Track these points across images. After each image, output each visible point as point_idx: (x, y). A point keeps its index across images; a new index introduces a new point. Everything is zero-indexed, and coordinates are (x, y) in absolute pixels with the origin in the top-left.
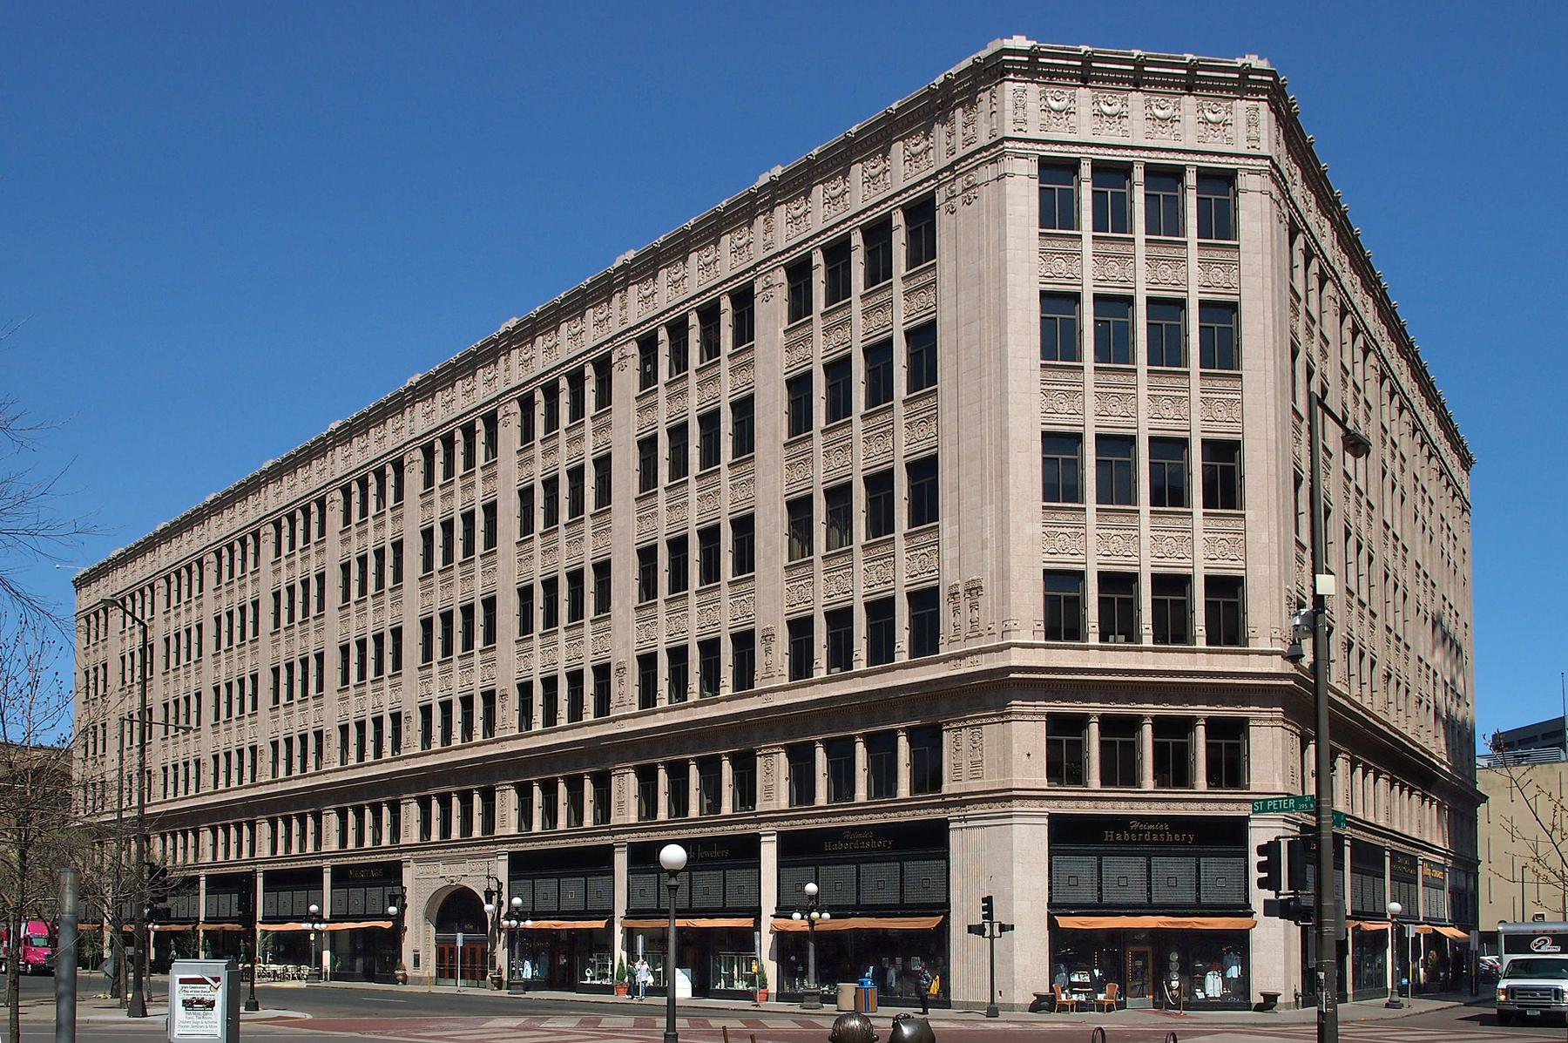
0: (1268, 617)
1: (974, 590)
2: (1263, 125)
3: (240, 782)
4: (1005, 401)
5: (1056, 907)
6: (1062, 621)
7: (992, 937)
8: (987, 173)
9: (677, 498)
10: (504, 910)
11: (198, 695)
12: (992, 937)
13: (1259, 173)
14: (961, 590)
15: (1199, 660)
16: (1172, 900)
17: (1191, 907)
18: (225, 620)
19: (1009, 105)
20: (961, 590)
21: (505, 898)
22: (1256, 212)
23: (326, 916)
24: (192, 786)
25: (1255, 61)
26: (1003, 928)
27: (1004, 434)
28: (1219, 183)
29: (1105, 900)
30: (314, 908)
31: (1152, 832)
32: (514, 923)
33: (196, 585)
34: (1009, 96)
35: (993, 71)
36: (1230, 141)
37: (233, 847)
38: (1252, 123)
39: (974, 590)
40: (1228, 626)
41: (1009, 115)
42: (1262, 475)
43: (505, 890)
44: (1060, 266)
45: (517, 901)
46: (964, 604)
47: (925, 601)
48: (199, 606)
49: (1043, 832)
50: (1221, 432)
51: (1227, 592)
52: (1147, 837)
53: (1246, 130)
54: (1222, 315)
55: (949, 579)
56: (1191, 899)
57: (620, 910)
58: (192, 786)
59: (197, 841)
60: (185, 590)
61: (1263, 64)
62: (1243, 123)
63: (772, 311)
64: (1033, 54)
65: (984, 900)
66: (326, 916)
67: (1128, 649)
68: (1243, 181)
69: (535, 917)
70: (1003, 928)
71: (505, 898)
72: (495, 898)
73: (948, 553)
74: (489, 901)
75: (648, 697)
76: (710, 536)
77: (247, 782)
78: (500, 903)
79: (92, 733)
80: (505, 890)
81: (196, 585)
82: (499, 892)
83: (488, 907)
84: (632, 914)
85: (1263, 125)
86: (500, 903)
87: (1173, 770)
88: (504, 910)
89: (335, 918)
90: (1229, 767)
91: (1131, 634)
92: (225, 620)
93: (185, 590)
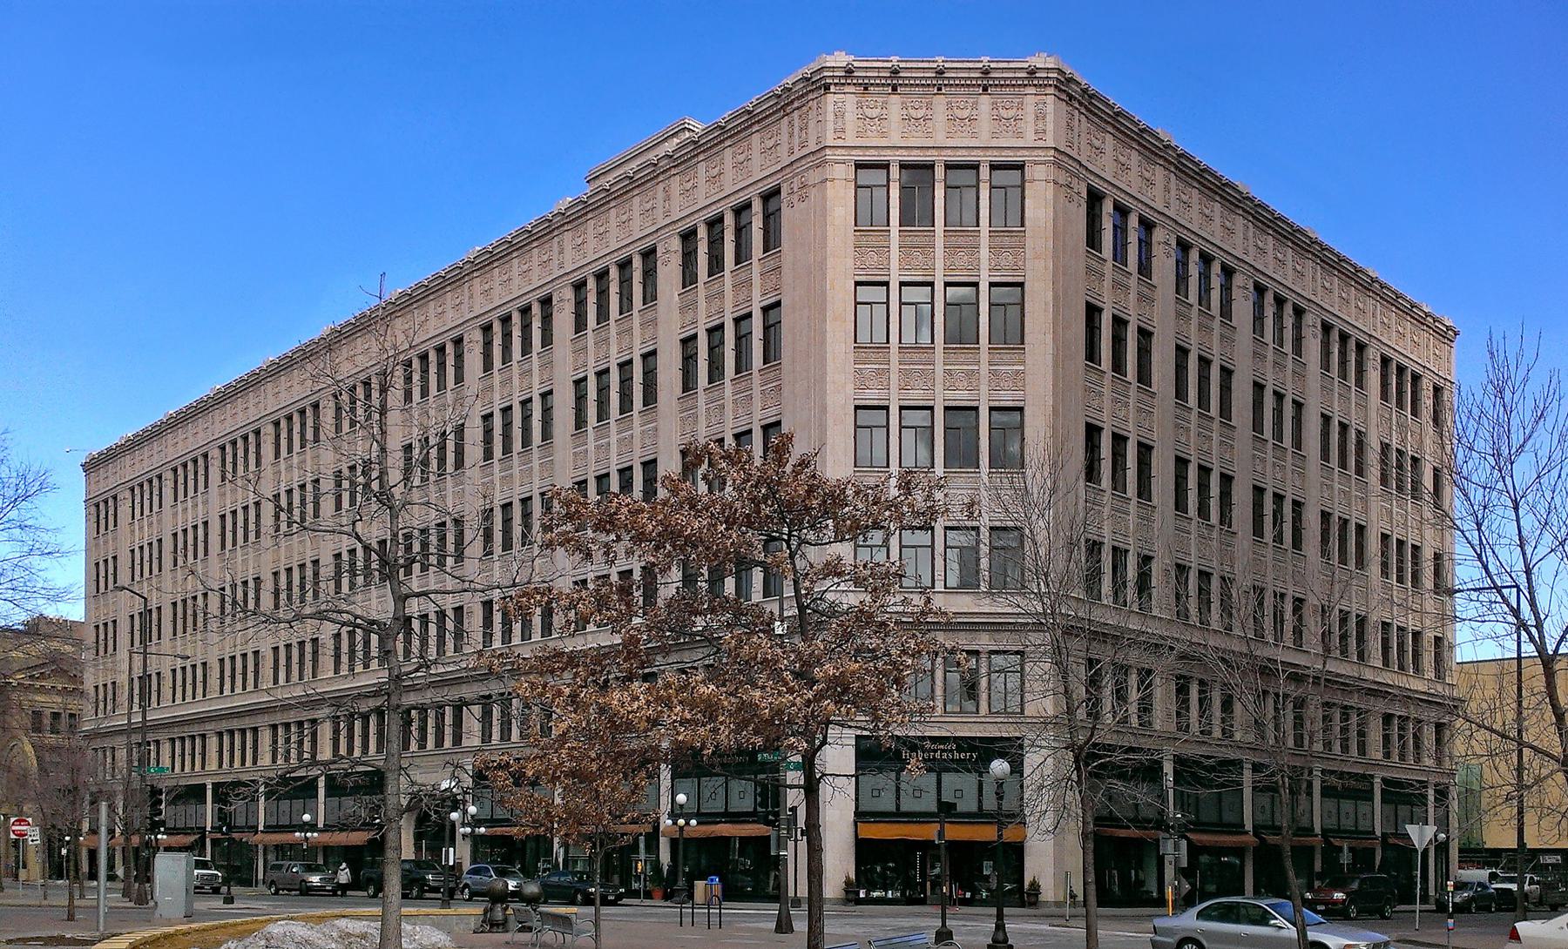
2: (1050, 118)
3: (244, 688)
5: (860, 816)
8: (813, 177)
11: (206, 523)
13: (1044, 163)
18: (229, 519)
19: (831, 117)
23: (321, 825)
24: (200, 690)
25: (1039, 61)
27: (824, 409)
29: (904, 808)
30: (307, 817)
31: (943, 751)
32: (468, 830)
33: (201, 479)
34: (830, 108)
35: (818, 85)
36: (1019, 135)
37: (358, 742)
38: (1040, 116)
41: (830, 126)
44: (873, 259)
48: (205, 502)
49: (852, 751)
50: (1006, 398)
52: (938, 755)
53: (1036, 124)
56: (890, 807)
58: (200, 690)
59: (204, 747)
60: (191, 483)
61: (1051, 63)
62: (1031, 118)
64: (849, 71)
66: (321, 825)
77: (250, 688)
79: (105, 631)
81: (201, 479)
85: (1050, 118)
89: (328, 828)
92: (229, 519)
93: (191, 483)
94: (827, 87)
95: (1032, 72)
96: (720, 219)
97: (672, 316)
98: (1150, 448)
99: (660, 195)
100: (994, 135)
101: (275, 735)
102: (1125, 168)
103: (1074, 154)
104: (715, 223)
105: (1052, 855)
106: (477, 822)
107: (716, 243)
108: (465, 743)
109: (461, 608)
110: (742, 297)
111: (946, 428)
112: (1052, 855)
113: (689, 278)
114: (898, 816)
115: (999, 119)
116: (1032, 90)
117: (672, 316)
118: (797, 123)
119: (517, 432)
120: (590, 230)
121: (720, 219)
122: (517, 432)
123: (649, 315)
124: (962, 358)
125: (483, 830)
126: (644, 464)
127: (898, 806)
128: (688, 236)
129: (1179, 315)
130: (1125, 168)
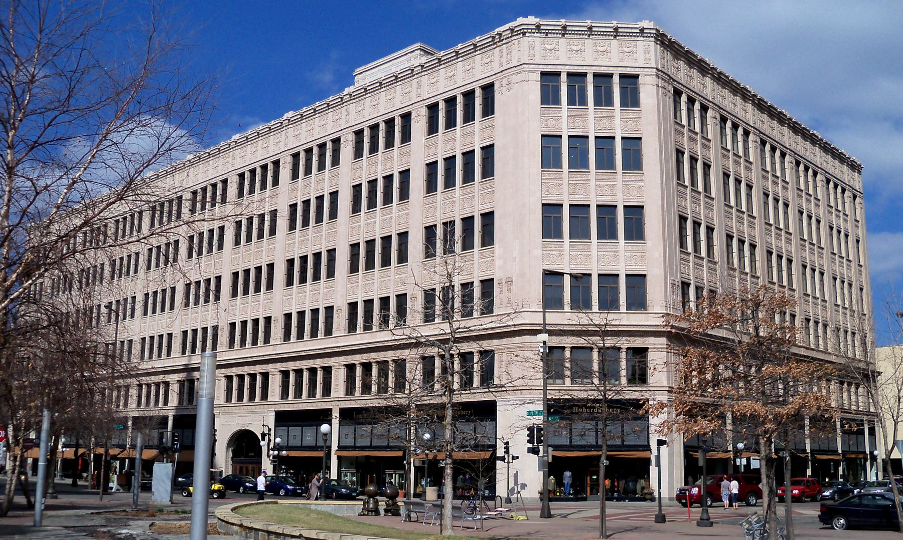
0: (659, 296)
1: (509, 282)
2: (653, 53)
4: (519, 190)
6: (551, 301)
7: (508, 463)
9: (370, 218)
10: (272, 445)
12: (508, 463)
14: (504, 281)
15: (623, 318)
16: (583, 443)
17: (619, 446)
20: (504, 281)
21: (272, 438)
22: (650, 92)
25: (646, 24)
26: (513, 458)
28: (630, 81)
39: (509, 282)
40: (638, 302)
42: (654, 222)
43: (272, 432)
45: (278, 440)
46: (505, 289)
47: (488, 285)
51: (637, 281)
52: (595, 410)
53: (643, 56)
54: (633, 144)
55: (497, 275)
57: (334, 447)
61: (651, 25)
63: (419, 126)
64: (538, 27)
65: (505, 444)
67: (666, 283)
68: (641, 79)
69: (288, 448)
70: (513, 458)
71: (272, 438)
72: (267, 438)
73: (498, 263)
74: (263, 439)
75: (352, 327)
76: (469, 155)
78: (270, 440)
80: (272, 432)
82: (269, 435)
83: (262, 443)
84: (341, 448)
86: (270, 440)
87: (608, 373)
88: (272, 445)
90: (639, 376)
91: (587, 305)
94: (524, 34)
95: (642, 30)
96: (324, 144)
97: (419, 152)
98: (713, 229)
99: (284, 137)
100: (622, 60)
101: (140, 390)
102: (691, 78)
103: (666, 71)
104: (309, 151)
105: (667, 475)
106: (278, 447)
107: (322, 156)
108: (269, 399)
109: (171, 334)
110: (449, 147)
111: (570, 217)
112: (667, 475)
113: (295, 176)
114: (354, 448)
115: (623, 52)
116: (642, 39)
117: (419, 152)
118: (505, 50)
119: (205, 244)
120: (271, 141)
121: (324, 144)
122: (205, 244)
123: (405, 150)
124: (607, 178)
125: (284, 453)
126: (445, 224)
127: (571, 442)
128: (296, 156)
129: (724, 156)
130: (691, 78)
